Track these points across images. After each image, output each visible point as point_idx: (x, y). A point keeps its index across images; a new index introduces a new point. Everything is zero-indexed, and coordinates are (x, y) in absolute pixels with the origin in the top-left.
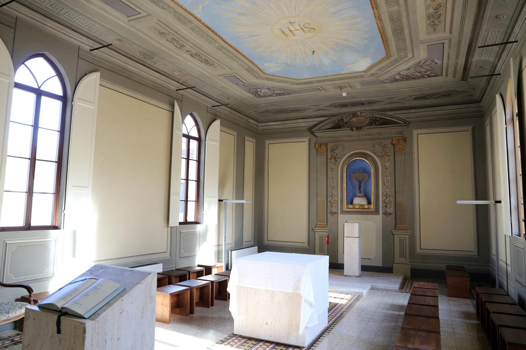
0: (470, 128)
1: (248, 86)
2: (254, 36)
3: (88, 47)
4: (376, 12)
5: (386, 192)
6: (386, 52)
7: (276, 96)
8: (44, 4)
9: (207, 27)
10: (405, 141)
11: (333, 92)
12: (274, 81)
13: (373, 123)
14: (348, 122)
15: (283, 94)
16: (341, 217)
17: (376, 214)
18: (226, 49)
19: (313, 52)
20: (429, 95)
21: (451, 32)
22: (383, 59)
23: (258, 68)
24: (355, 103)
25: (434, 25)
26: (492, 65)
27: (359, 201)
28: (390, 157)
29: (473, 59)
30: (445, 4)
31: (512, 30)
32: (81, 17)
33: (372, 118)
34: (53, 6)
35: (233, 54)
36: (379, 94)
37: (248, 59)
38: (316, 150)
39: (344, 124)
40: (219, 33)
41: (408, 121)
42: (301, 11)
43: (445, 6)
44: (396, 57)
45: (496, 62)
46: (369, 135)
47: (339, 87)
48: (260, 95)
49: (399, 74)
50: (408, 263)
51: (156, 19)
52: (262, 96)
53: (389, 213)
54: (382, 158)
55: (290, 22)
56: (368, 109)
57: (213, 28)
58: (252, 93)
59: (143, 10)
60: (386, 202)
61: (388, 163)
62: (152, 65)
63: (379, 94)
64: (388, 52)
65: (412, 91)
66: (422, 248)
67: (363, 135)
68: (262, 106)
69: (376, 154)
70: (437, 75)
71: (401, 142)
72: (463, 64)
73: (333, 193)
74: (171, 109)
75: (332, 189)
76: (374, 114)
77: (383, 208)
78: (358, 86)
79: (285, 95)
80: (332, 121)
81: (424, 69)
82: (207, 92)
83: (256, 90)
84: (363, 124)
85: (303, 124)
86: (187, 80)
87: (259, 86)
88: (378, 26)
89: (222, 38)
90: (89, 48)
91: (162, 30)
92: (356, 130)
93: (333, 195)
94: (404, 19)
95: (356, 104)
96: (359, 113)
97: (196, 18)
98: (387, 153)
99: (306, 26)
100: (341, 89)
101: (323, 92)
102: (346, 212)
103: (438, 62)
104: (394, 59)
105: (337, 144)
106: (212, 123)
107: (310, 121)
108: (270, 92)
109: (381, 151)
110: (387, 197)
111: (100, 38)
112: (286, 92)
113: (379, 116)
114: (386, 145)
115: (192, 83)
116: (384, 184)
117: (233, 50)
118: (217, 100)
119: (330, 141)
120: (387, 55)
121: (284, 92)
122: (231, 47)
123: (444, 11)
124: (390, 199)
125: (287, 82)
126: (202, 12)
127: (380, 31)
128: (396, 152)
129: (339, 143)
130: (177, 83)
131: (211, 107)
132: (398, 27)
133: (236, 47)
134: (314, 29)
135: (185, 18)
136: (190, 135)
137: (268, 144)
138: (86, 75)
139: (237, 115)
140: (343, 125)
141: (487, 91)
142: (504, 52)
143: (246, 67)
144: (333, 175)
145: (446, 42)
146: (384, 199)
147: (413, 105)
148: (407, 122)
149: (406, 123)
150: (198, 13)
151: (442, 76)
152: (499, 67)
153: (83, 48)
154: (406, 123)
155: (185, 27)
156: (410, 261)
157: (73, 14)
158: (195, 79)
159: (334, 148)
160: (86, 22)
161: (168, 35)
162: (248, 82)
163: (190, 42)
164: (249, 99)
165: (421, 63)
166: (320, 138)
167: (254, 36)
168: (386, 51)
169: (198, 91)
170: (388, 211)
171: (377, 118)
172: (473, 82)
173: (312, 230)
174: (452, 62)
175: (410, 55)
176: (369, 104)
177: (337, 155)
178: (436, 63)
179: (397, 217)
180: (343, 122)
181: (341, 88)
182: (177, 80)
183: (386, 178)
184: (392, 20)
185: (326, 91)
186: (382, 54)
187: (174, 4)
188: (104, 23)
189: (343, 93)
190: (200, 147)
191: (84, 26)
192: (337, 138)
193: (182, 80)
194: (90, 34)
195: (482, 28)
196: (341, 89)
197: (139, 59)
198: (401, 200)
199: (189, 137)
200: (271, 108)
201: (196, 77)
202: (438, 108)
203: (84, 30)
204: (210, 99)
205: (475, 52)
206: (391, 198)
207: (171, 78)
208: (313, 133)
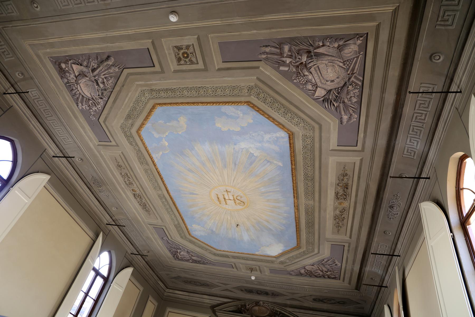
1: (171, 243)
2: (193, 194)
3: (53, 153)
4: (296, 202)
6: (297, 242)
7: (192, 262)
8: (40, 107)
9: (158, 173)
11: (243, 272)
12: (195, 245)
14: (250, 309)
15: (198, 262)
18: (166, 200)
19: (237, 225)
20: (326, 299)
22: (293, 248)
23: (186, 227)
24: (261, 291)
25: (339, 226)
26: (381, 278)
29: (366, 269)
30: (348, 209)
31: (396, 246)
32: (62, 128)
34: (46, 111)
35: (170, 206)
36: (283, 286)
37: (180, 215)
39: (246, 311)
40: (166, 182)
42: (238, 183)
43: (348, 212)
44: (305, 249)
45: (384, 275)
47: (250, 268)
48: (178, 257)
49: (305, 268)
51: (121, 152)
52: (180, 258)
55: (227, 191)
57: (163, 176)
58: (172, 253)
59: (115, 140)
62: (97, 192)
63: (283, 286)
64: (298, 242)
65: (313, 290)
68: (176, 269)
70: (336, 277)
72: (358, 272)
74: (94, 238)
76: (275, 307)
78: (267, 273)
79: (200, 263)
80: (235, 304)
81: (326, 268)
82: (132, 238)
83: (176, 250)
84: (264, 314)
85: (208, 300)
86: (120, 219)
87: (181, 247)
88: (295, 215)
89: (167, 187)
90: (53, 154)
91: (121, 163)
94: (316, 215)
95: (261, 293)
96: (261, 303)
97: (153, 162)
99: (239, 198)
100: (252, 271)
101: (235, 270)
103: (338, 264)
104: (303, 251)
106: (125, 268)
108: (187, 257)
111: (67, 151)
112: (202, 261)
113: (280, 310)
115: (122, 223)
117: (171, 202)
118: (138, 250)
120: (298, 245)
121: (200, 260)
122: (171, 198)
123: (347, 215)
125: (206, 250)
126: (160, 158)
127: (296, 220)
130: (110, 218)
131: (130, 254)
132: (311, 217)
133: (175, 200)
134: (243, 202)
135: (144, 158)
136: (100, 271)
137: (168, 312)
138: (38, 172)
139: (150, 272)
140: (244, 311)
141: (376, 305)
142: (390, 266)
143: (176, 223)
145: (347, 245)
147: (311, 307)
150: (157, 158)
151: (340, 280)
152: (386, 280)
153: (48, 152)
155: (141, 167)
157: (58, 123)
158: (127, 220)
160: (63, 133)
161: (124, 169)
162: (172, 238)
163: (138, 181)
164: (167, 259)
165: (324, 261)
167: (193, 194)
168: (297, 241)
169: (125, 234)
171: (278, 311)
172: (365, 293)
174: (349, 267)
175: (316, 251)
176: (273, 295)
178: (336, 265)
180: (245, 308)
181: (252, 270)
182: (112, 215)
184: (307, 213)
185: (238, 270)
186: (293, 244)
187: (141, 143)
188: (78, 139)
189: (253, 276)
190: (105, 287)
191: (60, 136)
193: (116, 217)
194: (61, 144)
195: (374, 240)
196: (252, 271)
197: (88, 182)
199: (98, 273)
200: (183, 275)
201: (129, 220)
203: (58, 139)
204: (131, 246)
205: (368, 261)
207: (107, 211)
208: (214, 312)
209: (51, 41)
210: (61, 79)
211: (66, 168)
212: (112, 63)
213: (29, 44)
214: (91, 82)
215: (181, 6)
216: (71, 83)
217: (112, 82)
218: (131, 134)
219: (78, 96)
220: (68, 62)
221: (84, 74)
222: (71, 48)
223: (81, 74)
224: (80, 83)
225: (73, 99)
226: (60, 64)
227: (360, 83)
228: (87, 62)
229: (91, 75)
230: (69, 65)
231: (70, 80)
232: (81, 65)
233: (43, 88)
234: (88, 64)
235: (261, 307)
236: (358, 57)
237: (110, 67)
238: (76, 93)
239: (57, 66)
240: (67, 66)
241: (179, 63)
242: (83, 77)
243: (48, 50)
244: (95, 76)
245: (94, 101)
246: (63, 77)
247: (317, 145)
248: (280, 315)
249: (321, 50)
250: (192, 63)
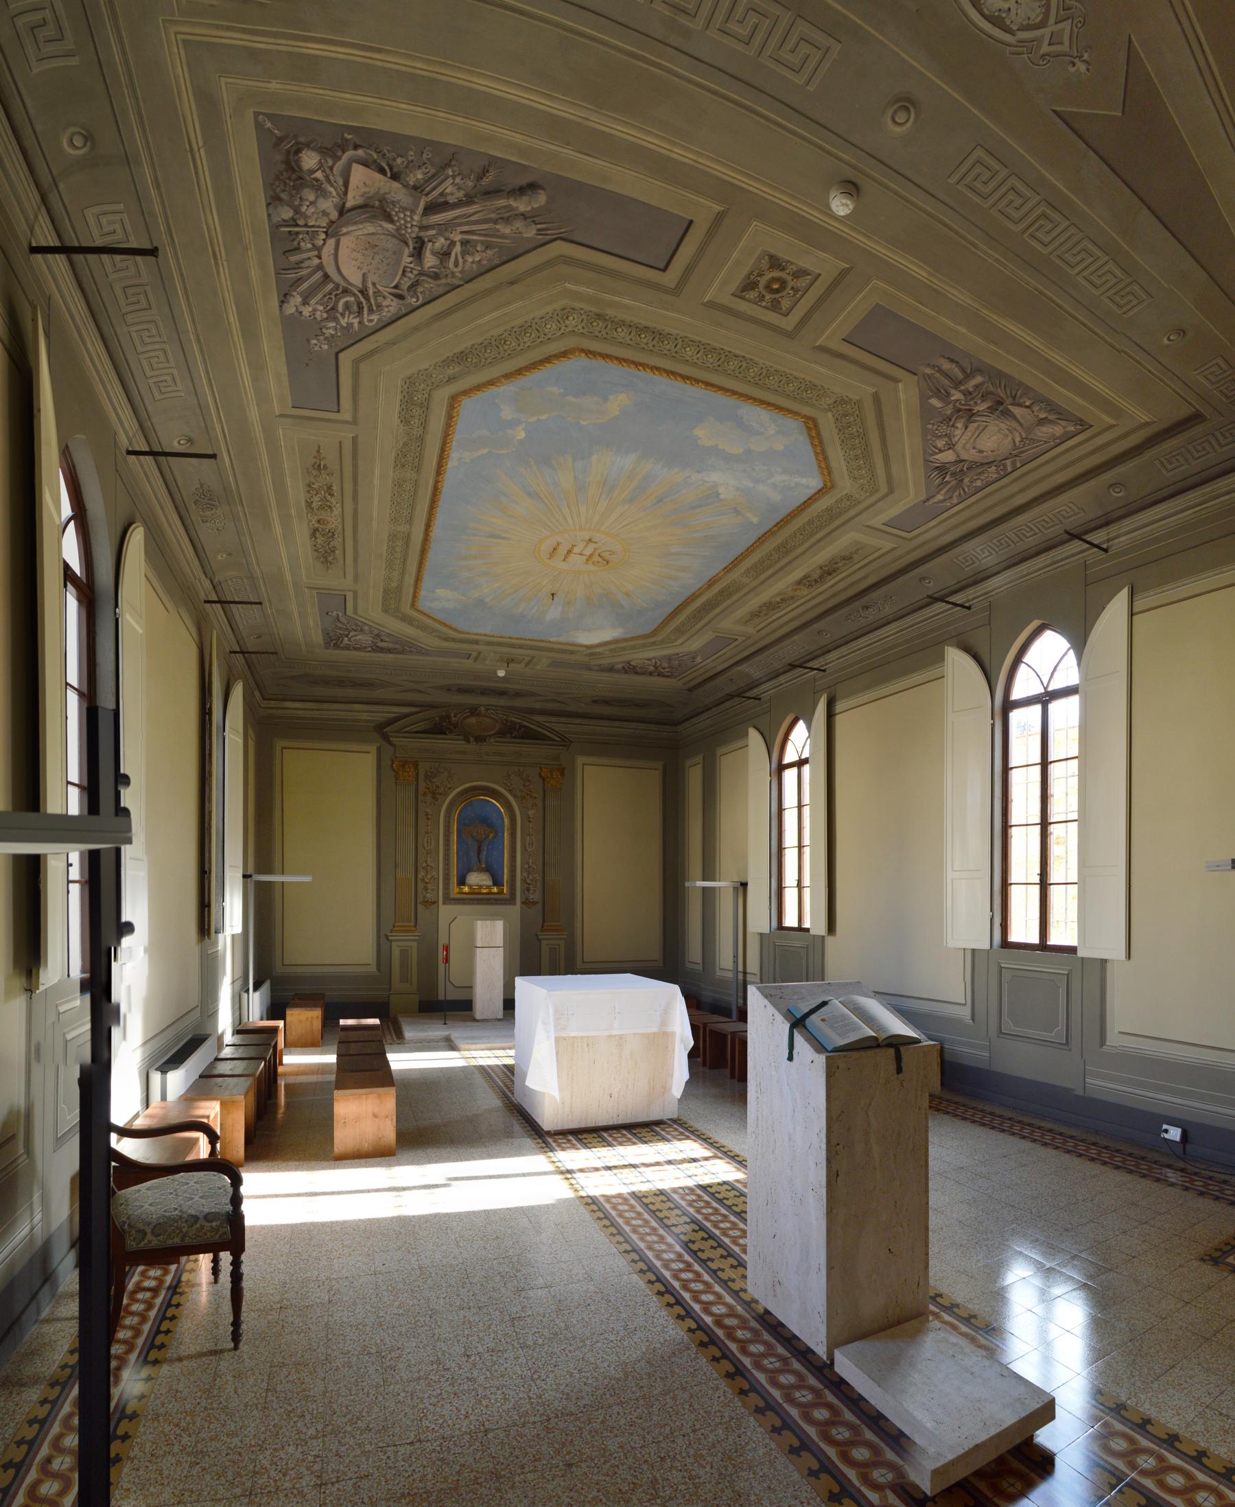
0: (660, 765)
10: (562, 774)
15: (389, 651)
16: (445, 911)
17: (510, 904)
19: (553, 595)
21: (758, 631)
27: (477, 879)
38: (394, 774)
77: (523, 892)
85: (364, 714)
96: (482, 709)
102: (455, 899)
143: (394, 585)
171: (515, 723)
177: (437, 787)
184: (721, 592)
202: (617, 723)
208: (385, 737)
209: (312, 49)
210: (268, 205)
211: (146, 475)
212: (529, 208)
213: (184, 41)
214: (396, 241)
215: (887, 187)
216: (306, 225)
217: (480, 261)
218: (428, 400)
219: (304, 272)
220: (339, 153)
221: (385, 211)
222: (394, 104)
223: (373, 207)
224: (343, 235)
225: (276, 278)
226: (298, 151)
227: (1009, 469)
228: (429, 174)
229: (412, 218)
230: (339, 165)
231: (306, 217)
232: (395, 177)
233: (168, 225)
234: (426, 181)
236: (1046, 442)
237: (508, 218)
238: (302, 262)
239: (279, 157)
240: (330, 163)
241: (743, 291)
242: (374, 217)
243: (274, 85)
244: (423, 228)
245: (362, 300)
246: (280, 199)
247: (852, 513)
249: (1017, 411)
250: (775, 306)
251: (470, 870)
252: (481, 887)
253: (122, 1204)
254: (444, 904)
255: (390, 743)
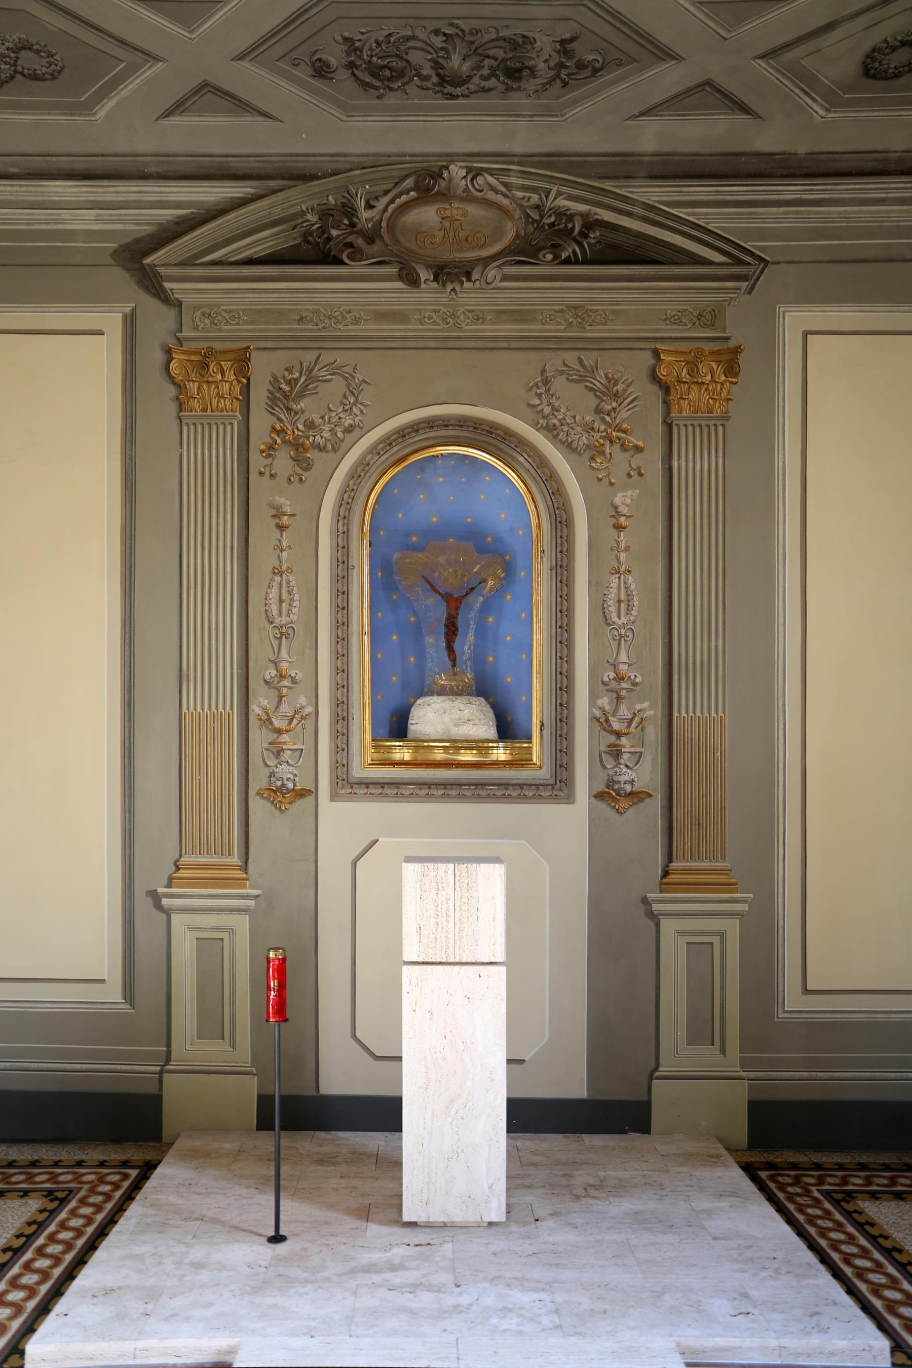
5: (615, 666)
10: (732, 369)
13: (539, 250)
17: (555, 798)
28: (639, 455)
33: (537, 217)
38: (172, 390)
39: (360, 242)
41: (752, 254)
46: (519, 316)
50: (738, 1070)
53: (632, 794)
54: (592, 459)
56: (519, 146)
60: (616, 726)
61: (630, 493)
66: (809, 988)
67: (479, 318)
69: (555, 437)
71: (709, 370)
73: (284, 665)
75: (275, 643)
77: (597, 761)
80: (278, 213)
84: (482, 247)
92: (436, 279)
93: (286, 683)
98: (625, 432)
105: (309, 357)
107: (132, 197)
109: (588, 418)
110: (619, 698)
113: (583, 208)
114: (620, 387)
116: (600, 614)
119: (267, 338)
124: (638, 707)
128: (675, 429)
129: (327, 357)
140: (350, 245)
144: (285, 555)
146: (602, 709)
148: (748, 259)
149: (740, 262)
154: (740, 262)
156: (744, 1063)
159: (289, 383)
166: (198, 314)
170: (623, 778)
171: (571, 218)
173: (150, 901)
177: (310, 425)
179: (677, 814)
183: (614, 579)
192: (311, 321)
198: (698, 713)
206: (646, 704)
235: (456, 205)
248: (586, 236)
251: (425, 690)
252: (456, 744)
253: (47, 1151)
254: (334, 797)
255: (164, 297)
